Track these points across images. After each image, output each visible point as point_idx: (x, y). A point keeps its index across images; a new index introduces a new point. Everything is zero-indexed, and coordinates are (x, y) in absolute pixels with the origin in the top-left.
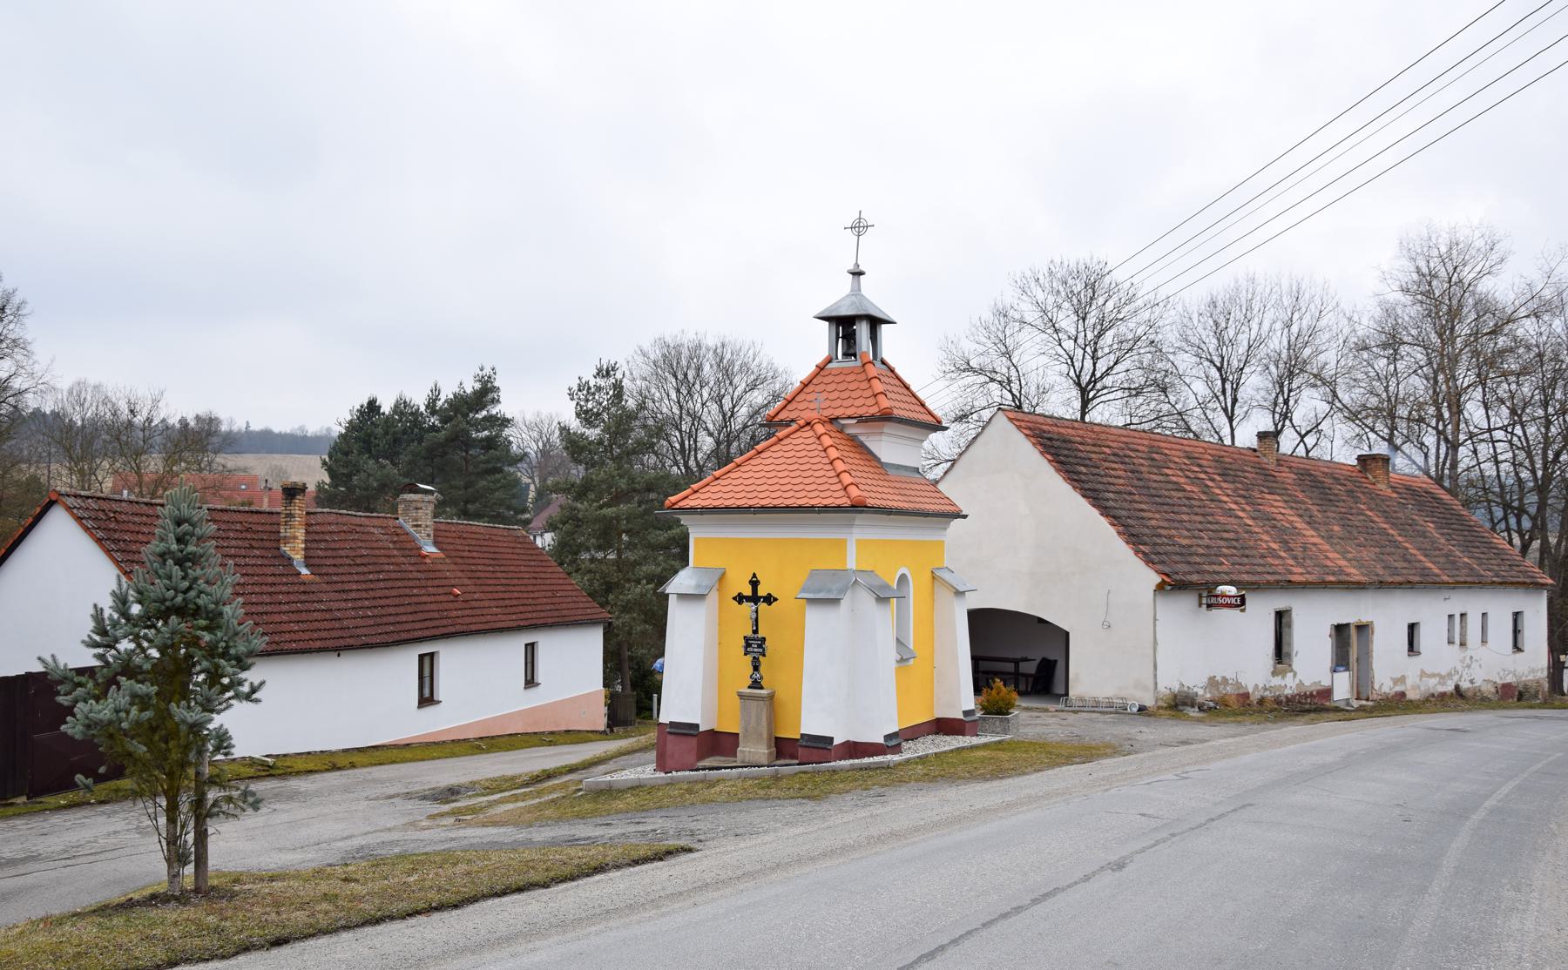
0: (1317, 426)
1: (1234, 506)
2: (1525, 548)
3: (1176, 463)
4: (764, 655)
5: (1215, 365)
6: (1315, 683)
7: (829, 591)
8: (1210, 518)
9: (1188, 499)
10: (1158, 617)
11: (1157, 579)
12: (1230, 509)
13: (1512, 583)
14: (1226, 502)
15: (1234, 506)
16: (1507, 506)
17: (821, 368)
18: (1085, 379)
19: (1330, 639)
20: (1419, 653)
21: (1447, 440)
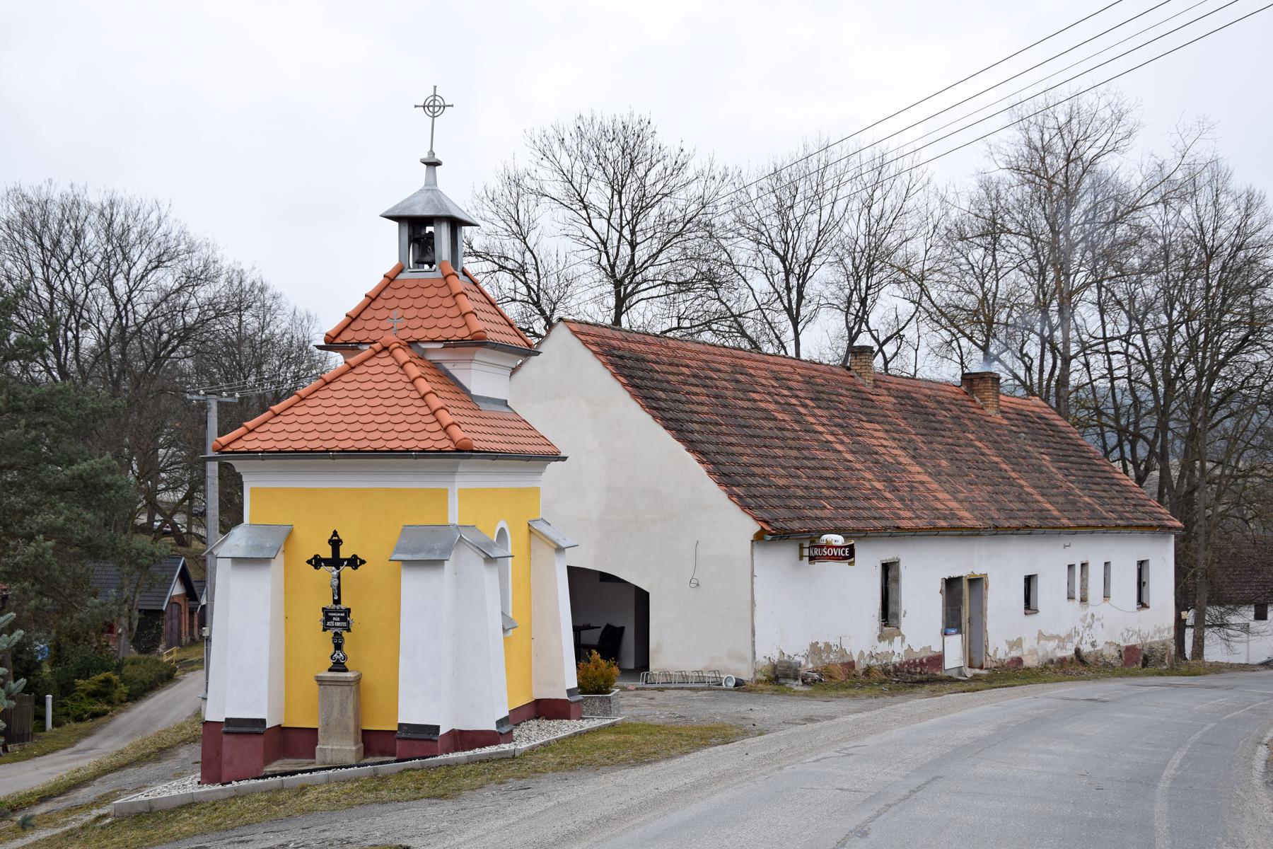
0: (898, 332)
1: (831, 438)
2: (1140, 480)
3: (763, 385)
4: (349, 630)
5: (777, 254)
6: (924, 648)
7: (430, 551)
8: (806, 453)
9: (780, 429)
10: (755, 573)
11: (755, 527)
12: (828, 442)
13: (1138, 527)
14: (821, 433)
15: (831, 438)
16: (1121, 432)
17: (390, 279)
18: (620, 270)
19: (941, 596)
20: (1036, 611)
21: (1054, 349)
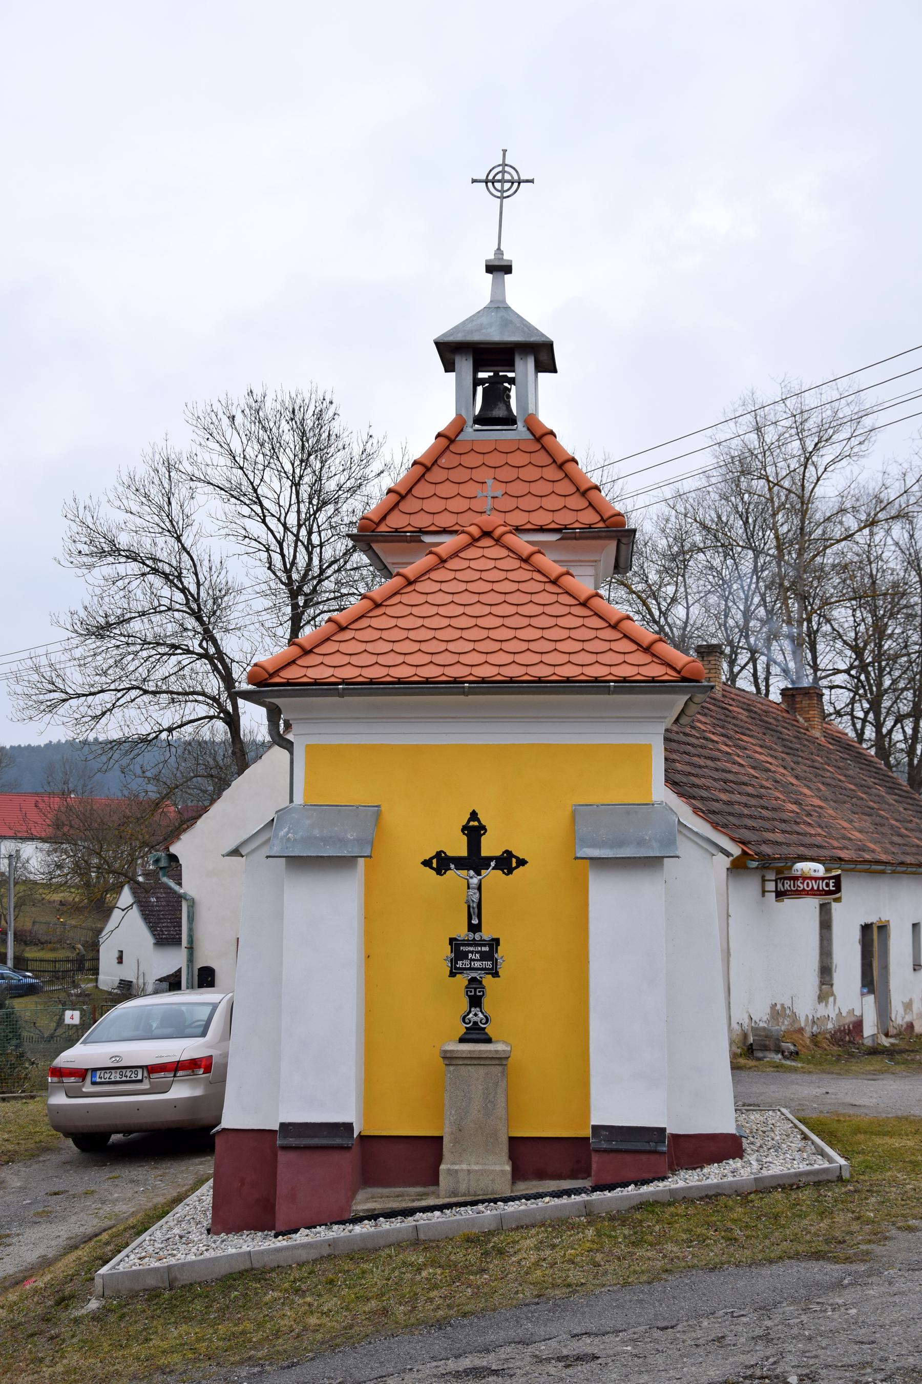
4: (496, 974)
7: (641, 843)
